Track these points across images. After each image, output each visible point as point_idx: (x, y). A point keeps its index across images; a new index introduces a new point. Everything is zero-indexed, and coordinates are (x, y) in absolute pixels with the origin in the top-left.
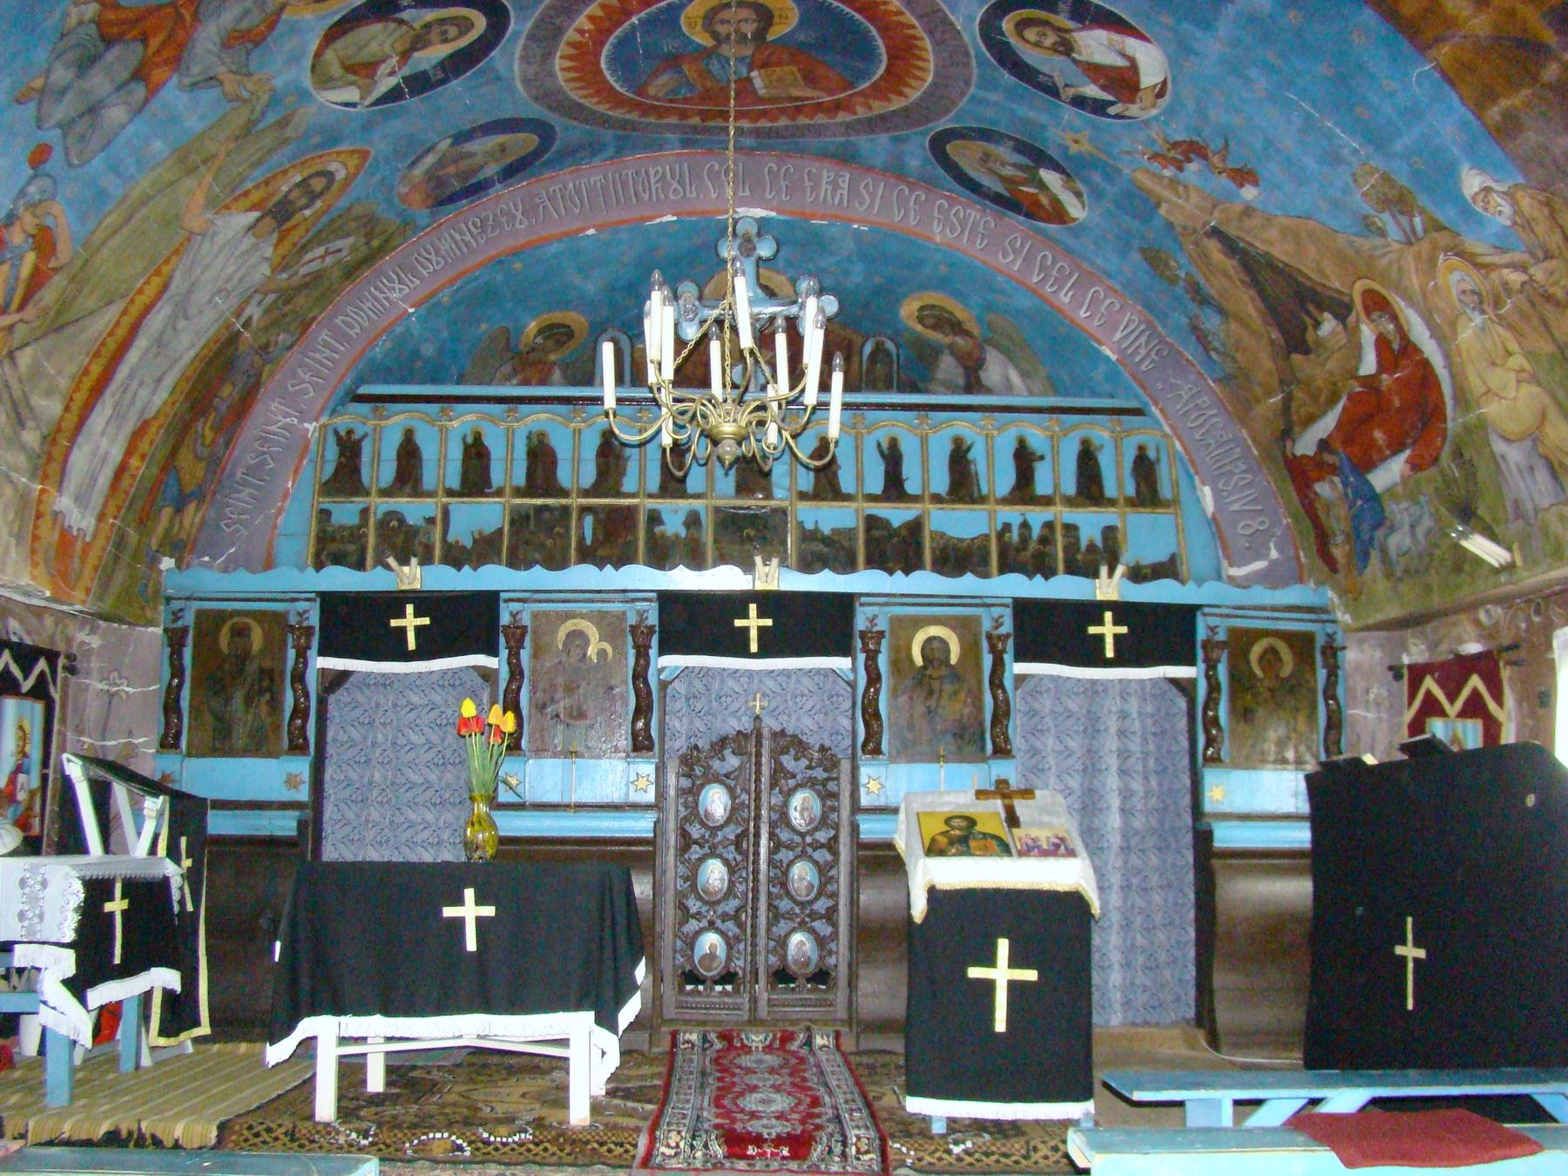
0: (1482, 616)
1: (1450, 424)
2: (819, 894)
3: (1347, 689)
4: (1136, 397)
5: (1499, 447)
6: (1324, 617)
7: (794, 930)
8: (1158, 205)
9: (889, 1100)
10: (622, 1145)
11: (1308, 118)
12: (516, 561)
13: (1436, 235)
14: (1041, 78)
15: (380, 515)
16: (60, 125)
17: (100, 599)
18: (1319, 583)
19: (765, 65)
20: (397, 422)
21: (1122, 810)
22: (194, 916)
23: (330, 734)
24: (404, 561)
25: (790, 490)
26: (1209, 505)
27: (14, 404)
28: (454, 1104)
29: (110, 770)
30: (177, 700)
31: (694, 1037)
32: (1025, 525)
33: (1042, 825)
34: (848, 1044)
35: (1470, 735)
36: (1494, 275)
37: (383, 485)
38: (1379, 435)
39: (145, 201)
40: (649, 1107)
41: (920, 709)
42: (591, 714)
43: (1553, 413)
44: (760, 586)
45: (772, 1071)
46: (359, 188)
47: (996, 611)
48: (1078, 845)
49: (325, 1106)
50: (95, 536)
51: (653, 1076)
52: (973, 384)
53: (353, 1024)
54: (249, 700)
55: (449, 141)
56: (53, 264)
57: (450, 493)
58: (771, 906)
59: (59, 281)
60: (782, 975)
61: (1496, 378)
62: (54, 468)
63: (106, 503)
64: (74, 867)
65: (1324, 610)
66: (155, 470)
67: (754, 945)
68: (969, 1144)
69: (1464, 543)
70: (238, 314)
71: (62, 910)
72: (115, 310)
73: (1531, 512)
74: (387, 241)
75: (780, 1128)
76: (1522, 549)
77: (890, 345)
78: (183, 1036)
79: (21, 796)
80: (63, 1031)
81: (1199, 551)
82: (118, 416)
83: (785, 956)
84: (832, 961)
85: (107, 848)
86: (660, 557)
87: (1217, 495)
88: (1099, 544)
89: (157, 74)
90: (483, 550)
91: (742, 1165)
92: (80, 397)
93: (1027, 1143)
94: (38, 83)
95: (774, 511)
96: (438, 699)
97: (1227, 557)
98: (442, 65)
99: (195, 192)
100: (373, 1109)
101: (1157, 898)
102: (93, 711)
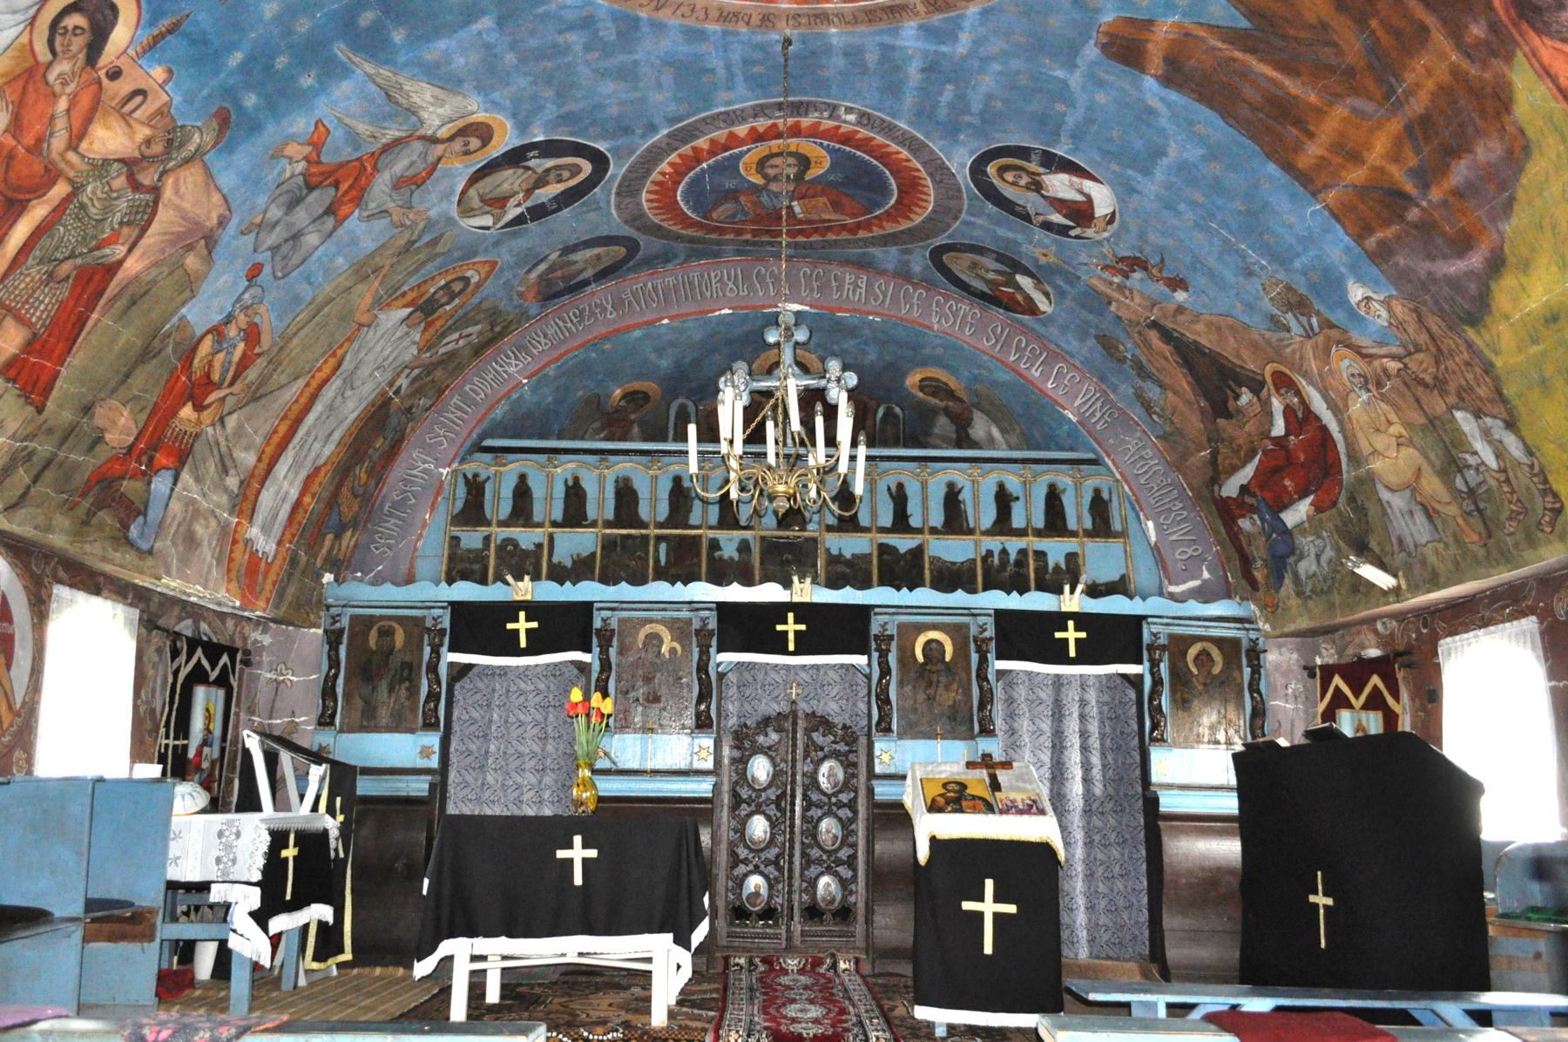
0: (1379, 626)
2: (842, 843)
3: (1268, 684)
4: (1093, 451)
5: (1385, 495)
7: (822, 874)
8: (1110, 303)
9: (900, 1011)
11: (1226, 241)
12: (608, 579)
14: (1018, 209)
16: (269, 249)
18: (1242, 599)
20: (512, 469)
22: (345, 861)
23: (456, 713)
24: (519, 578)
25: (819, 523)
26: (1153, 538)
28: (557, 1012)
29: (277, 742)
30: (334, 687)
31: (742, 961)
32: (1004, 552)
33: (1019, 789)
34: (866, 969)
35: (1374, 723)
36: (1376, 363)
39: (329, 301)
40: (712, 1014)
41: (921, 697)
43: (1426, 469)
44: (796, 599)
45: (806, 988)
46: (490, 288)
47: (981, 620)
48: (1049, 808)
49: (458, 1010)
50: (275, 557)
51: (711, 991)
52: (963, 440)
53: (482, 945)
54: (391, 690)
56: (257, 350)
57: (555, 524)
58: (804, 854)
59: (261, 363)
60: (813, 912)
61: (1380, 442)
62: (247, 506)
63: (283, 534)
65: (1249, 621)
66: (322, 506)
67: (790, 885)
70: (391, 384)
72: (301, 382)
73: (1412, 547)
74: (505, 327)
77: (897, 410)
78: (331, 961)
79: (205, 765)
80: (247, 954)
81: (1145, 574)
82: (296, 465)
84: (852, 899)
85: (276, 810)
87: (1158, 527)
88: (1063, 567)
89: (344, 210)
90: (580, 570)
92: (269, 450)
94: (258, 220)
95: (808, 539)
96: (542, 686)
98: (556, 198)
99: (364, 295)
101: (1115, 853)
102: (263, 695)
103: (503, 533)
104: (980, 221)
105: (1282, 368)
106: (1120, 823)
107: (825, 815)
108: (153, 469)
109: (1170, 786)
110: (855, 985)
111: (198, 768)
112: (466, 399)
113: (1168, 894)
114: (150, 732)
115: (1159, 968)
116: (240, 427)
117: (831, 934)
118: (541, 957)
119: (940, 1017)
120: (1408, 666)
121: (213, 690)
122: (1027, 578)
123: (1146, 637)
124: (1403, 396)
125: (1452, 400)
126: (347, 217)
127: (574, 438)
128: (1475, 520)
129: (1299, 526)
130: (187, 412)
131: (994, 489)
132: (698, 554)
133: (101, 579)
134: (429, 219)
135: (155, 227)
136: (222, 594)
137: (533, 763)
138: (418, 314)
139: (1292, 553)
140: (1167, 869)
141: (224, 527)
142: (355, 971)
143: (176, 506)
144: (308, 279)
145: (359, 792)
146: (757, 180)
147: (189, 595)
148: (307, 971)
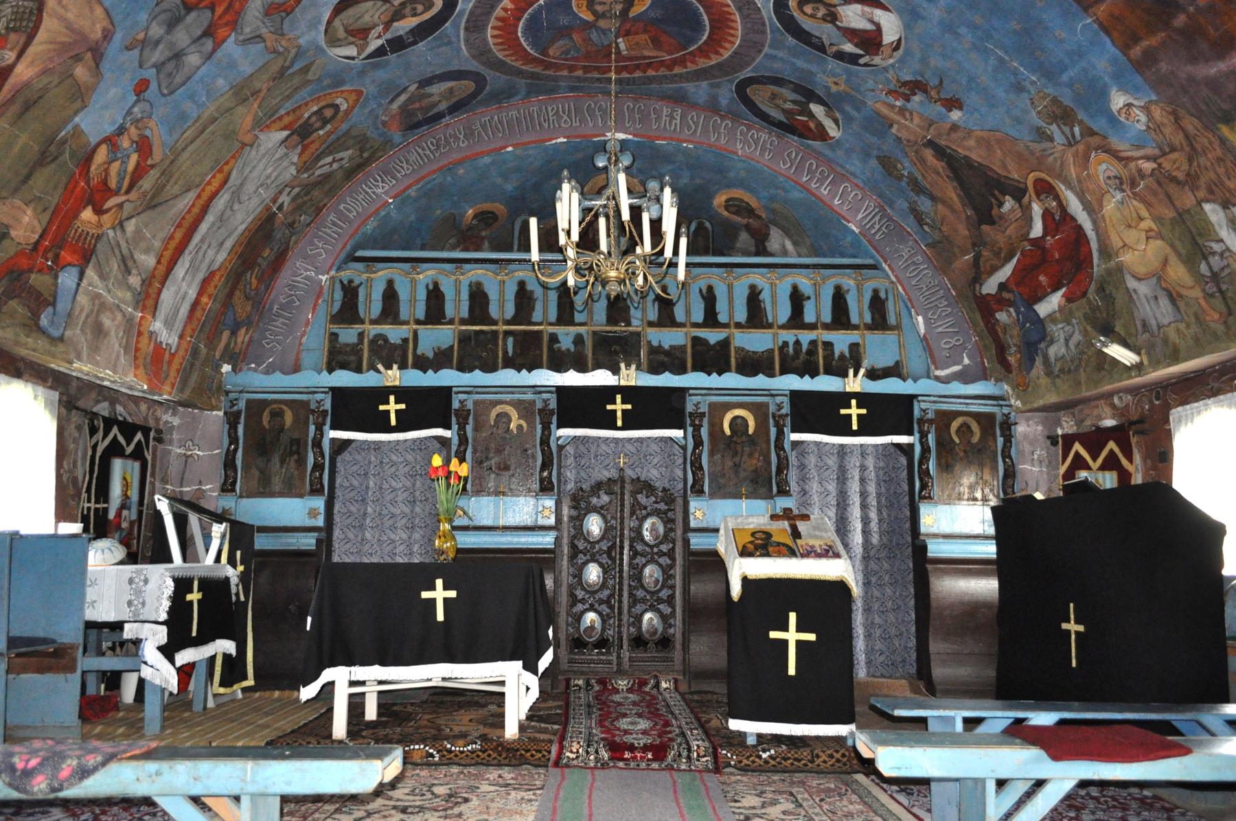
0: (1116, 400)
1: (1095, 269)
2: (663, 587)
3: (1018, 452)
4: (872, 257)
5: (1132, 283)
6: (1001, 402)
7: (646, 611)
8: (891, 126)
9: (715, 723)
10: (540, 752)
11: (1001, 61)
13: (1090, 139)
14: (814, 40)
15: (371, 337)
16: (155, 66)
17: (182, 390)
18: (997, 381)
19: (627, 34)
20: (382, 274)
21: (864, 532)
23: (338, 481)
24: (389, 367)
26: (922, 329)
27: (124, 260)
28: (426, 727)
29: (185, 507)
31: (581, 682)
32: (797, 343)
33: (817, 537)
34: (683, 687)
35: (1108, 481)
36: (1132, 165)
37: (373, 317)
38: (1042, 278)
39: (213, 120)
40: (556, 727)
42: (512, 468)
43: (1173, 259)
44: (623, 383)
45: (634, 704)
46: (356, 116)
47: (779, 399)
49: (340, 727)
52: (761, 250)
53: (360, 672)
54: (282, 462)
55: (416, 85)
56: (149, 162)
57: (418, 322)
58: (631, 595)
59: (154, 174)
60: (639, 642)
62: (150, 302)
63: (185, 326)
64: (166, 569)
65: (1002, 398)
66: (218, 306)
67: (620, 620)
68: (773, 752)
69: (1105, 350)
70: (274, 201)
71: (159, 599)
72: (191, 196)
73: (1155, 328)
74: (374, 153)
75: (644, 741)
76: (1148, 354)
77: (708, 224)
78: (235, 687)
79: (124, 525)
80: (157, 682)
81: (915, 359)
82: (193, 269)
83: (640, 627)
84: (672, 631)
85: (185, 560)
86: (558, 365)
87: (927, 322)
89: (222, 32)
90: (440, 360)
91: (621, 764)
93: (812, 752)
94: (141, 36)
95: (632, 333)
96: (410, 458)
97: (934, 363)
98: (412, 31)
99: (245, 116)
100: (371, 731)
102: (174, 468)
103: (374, 330)
104: (780, 54)
105: (1043, 175)
106: (892, 566)
107: (648, 563)
108: (59, 265)
109: (936, 536)
110: (675, 701)
111: (118, 527)
112: (342, 216)
113: (934, 623)
114: (73, 497)
115: (925, 682)
116: (138, 231)
117: (653, 659)
118: (413, 682)
119: (750, 728)
120: (1140, 433)
121: (130, 462)
122: (817, 364)
123: (917, 413)
124: (1155, 194)
125: (1201, 194)
126: (224, 41)
127: (434, 249)
128: (1218, 302)
129: (1051, 317)
130: (87, 214)
131: (789, 290)
132: (540, 347)
133: (21, 365)
134: (299, 47)
135: (41, 35)
136: (130, 378)
137: (404, 521)
138: (295, 137)
139: (1043, 339)
140: (934, 604)
141: (129, 320)
142: (257, 695)
143: (82, 299)
144: (192, 97)
145: (257, 547)
146: (588, 17)
147: (102, 379)
148: (215, 695)
